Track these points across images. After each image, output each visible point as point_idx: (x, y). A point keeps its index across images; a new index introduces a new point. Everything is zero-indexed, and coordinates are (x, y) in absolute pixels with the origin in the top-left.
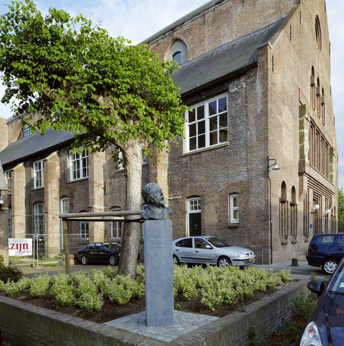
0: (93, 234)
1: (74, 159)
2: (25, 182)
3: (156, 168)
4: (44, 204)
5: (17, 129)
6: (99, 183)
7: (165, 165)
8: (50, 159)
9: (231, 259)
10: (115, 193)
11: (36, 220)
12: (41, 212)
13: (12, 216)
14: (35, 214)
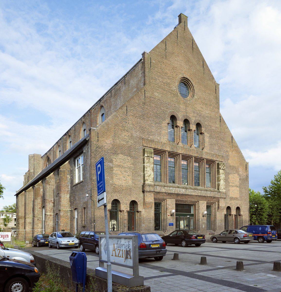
8: (37, 185)
9: (59, 243)
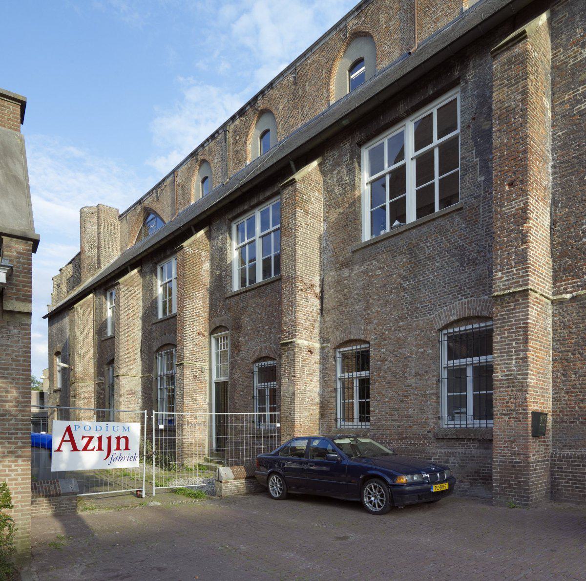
0: (292, 413)
1: (243, 240)
2: (141, 308)
3: (525, 193)
4: (176, 350)
5: (136, 223)
6: (307, 282)
7: (545, 188)
8: (190, 245)
10: (352, 304)
11: (162, 385)
12: (170, 366)
13: (115, 376)
14: (159, 373)
